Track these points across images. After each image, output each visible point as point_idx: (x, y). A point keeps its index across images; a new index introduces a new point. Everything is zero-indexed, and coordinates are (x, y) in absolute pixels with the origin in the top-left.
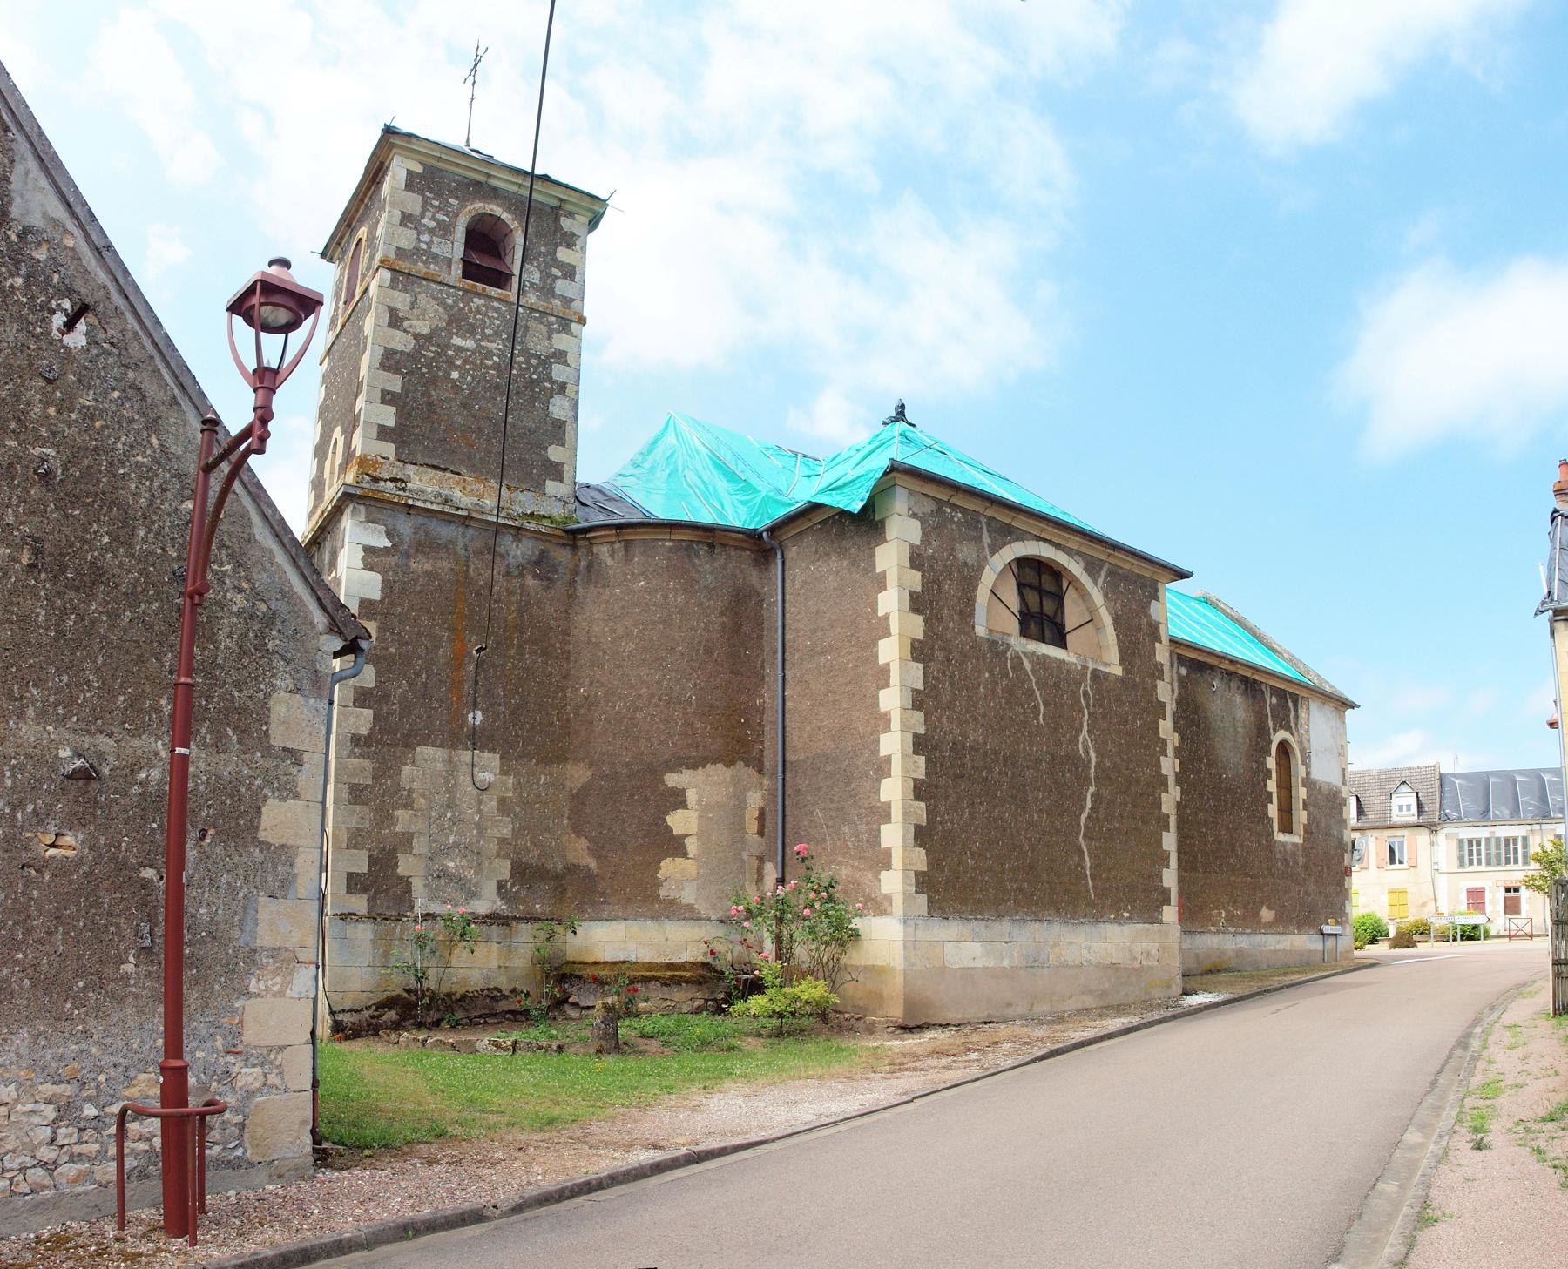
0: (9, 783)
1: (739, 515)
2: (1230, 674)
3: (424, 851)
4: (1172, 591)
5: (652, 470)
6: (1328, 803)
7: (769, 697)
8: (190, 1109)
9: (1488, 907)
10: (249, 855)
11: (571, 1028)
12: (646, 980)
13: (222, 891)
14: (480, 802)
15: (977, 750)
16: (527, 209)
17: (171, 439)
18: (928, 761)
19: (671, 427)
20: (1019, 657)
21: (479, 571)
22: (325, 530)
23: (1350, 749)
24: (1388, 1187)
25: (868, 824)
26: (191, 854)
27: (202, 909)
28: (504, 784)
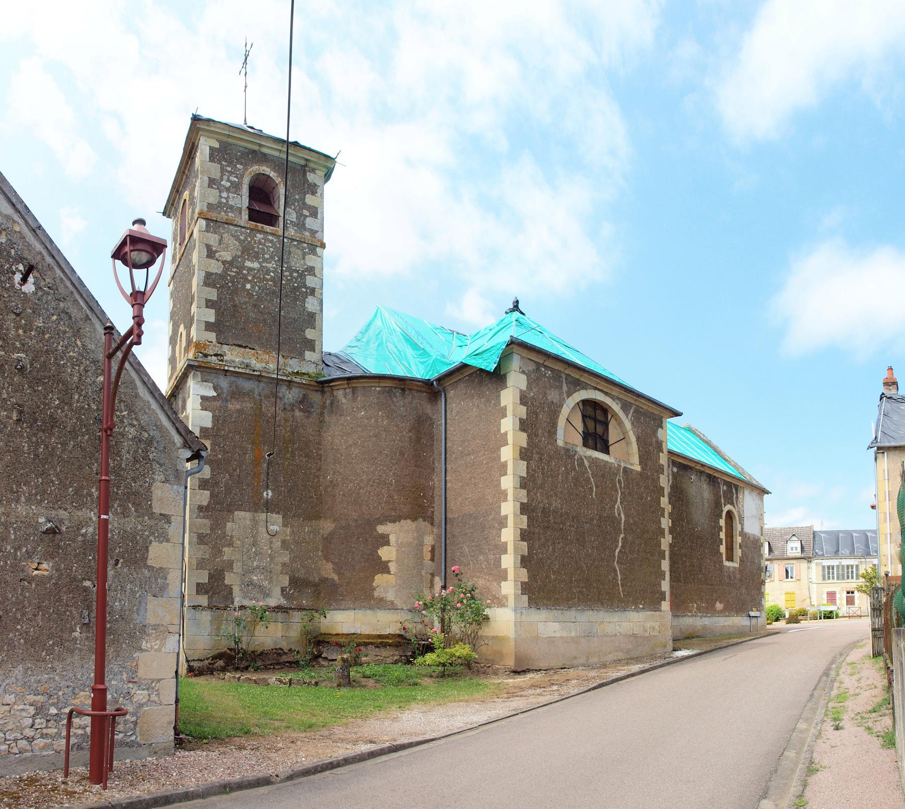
0: (13, 537)
1: (420, 371)
2: (701, 472)
3: (240, 571)
4: (671, 423)
5: (368, 342)
6: (753, 545)
7: (437, 480)
8: (108, 712)
9: (838, 602)
10: (142, 573)
11: (323, 672)
12: (366, 644)
13: (127, 593)
14: (271, 543)
15: (557, 512)
16: (286, 168)
17: (88, 341)
18: (529, 518)
19: (379, 315)
20: (581, 459)
21: (268, 408)
22: (179, 387)
23: (766, 517)
24: (791, 754)
25: (494, 554)
26: (111, 573)
27: (116, 603)
28: (285, 532)
